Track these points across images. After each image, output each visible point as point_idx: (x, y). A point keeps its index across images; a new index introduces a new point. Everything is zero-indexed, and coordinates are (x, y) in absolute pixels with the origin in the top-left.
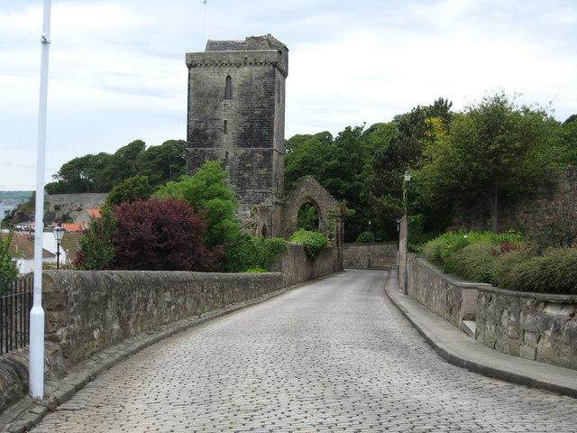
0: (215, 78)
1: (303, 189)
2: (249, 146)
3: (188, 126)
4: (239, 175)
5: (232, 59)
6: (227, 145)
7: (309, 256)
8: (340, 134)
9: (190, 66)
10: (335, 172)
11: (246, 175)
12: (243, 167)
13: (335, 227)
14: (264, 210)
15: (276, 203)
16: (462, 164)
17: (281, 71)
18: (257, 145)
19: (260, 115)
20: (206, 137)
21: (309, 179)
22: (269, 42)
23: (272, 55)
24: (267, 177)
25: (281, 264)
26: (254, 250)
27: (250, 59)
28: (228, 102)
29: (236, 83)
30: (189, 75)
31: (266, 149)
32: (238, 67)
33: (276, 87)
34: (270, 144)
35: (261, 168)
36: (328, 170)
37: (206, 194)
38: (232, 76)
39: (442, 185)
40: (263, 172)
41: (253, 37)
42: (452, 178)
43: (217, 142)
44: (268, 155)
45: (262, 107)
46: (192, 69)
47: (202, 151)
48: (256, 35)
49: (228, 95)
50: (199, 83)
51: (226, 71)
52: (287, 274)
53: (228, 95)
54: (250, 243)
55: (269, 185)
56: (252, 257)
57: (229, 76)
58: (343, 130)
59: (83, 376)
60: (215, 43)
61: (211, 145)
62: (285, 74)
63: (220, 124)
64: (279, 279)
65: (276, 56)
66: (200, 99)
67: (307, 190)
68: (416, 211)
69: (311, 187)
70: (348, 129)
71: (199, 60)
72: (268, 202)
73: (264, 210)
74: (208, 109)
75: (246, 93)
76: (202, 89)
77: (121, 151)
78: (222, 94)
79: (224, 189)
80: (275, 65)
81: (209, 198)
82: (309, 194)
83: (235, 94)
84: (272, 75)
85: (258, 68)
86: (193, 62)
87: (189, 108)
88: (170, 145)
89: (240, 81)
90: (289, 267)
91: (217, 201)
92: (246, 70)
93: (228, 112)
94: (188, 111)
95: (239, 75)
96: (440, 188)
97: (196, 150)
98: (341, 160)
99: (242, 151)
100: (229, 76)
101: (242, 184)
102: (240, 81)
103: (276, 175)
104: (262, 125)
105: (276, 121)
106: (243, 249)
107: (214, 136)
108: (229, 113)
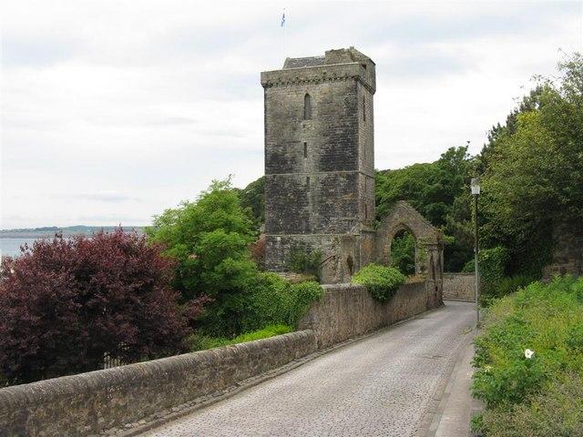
0: (293, 97)
1: (396, 216)
2: (332, 170)
3: (266, 150)
4: (321, 202)
5: (311, 75)
6: (308, 172)
7: (375, 299)
8: (442, 155)
9: (265, 86)
10: (433, 197)
11: (330, 202)
12: (326, 193)
13: (429, 257)
14: (348, 241)
15: (364, 232)
16: (560, 157)
17: (366, 86)
18: (341, 169)
19: (343, 135)
20: (285, 162)
21: (403, 204)
22: (352, 54)
23: (354, 68)
24: (353, 204)
25: (312, 319)
26: (276, 299)
27: (329, 74)
28: (308, 123)
29: (315, 102)
30: (265, 95)
31: (350, 172)
32: (317, 83)
33: (360, 103)
34: (354, 166)
35: (346, 193)
36: (430, 195)
37: (207, 224)
38: (310, 93)
39: (526, 198)
40: (347, 197)
41: (332, 50)
42: (544, 184)
43: (296, 167)
44: (352, 179)
45: (345, 126)
46: (269, 89)
47: (281, 177)
48: (336, 48)
49: (307, 115)
50: (276, 103)
51: (304, 89)
52: (321, 332)
53: (307, 116)
54: (271, 290)
55: (355, 212)
56: (273, 309)
57: (307, 95)
58: (445, 151)
59: (298, 364)
60: (294, 60)
61: (290, 170)
62: (372, 90)
63: (299, 147)
64: (310, 339)
65: (358, 68)
66: (278, 123)
67: (401, 216)
68: (492, 243)
69: (405, 214)
70: (452, 150)
71: (274, 79)
72: (354, 231)
73: (348, 241)
74: (287, 131)
75: (328, 110)
76: (278, 110)
77: (251, 185)
78: (301, 114)
79: (231, 217)
80: (357, 79)
81: (212, 229)
82: (403, 220)
83: (315, 114)
84: (355, 90)
85: (338, 84)
86: (269, 81)
87: (266, 131)
88: (260, 180)
89: (323, 105)
90: (323, 322)
91: (219, 233)
92: (325, 86)
93: (308, 133)
94: (266, 135)
95: (318, 93)
96: (523, 202)
97: (274, 177)
98: (445, 182)
99: (325, 175)
100: (307, 95)
101: (326, 211)
102: (323, 105)
103: (363, 201)
104: (345, 146)
105: (361, 141)
106: (259, 301)
107: (293, 159)
108: (309, 134)
